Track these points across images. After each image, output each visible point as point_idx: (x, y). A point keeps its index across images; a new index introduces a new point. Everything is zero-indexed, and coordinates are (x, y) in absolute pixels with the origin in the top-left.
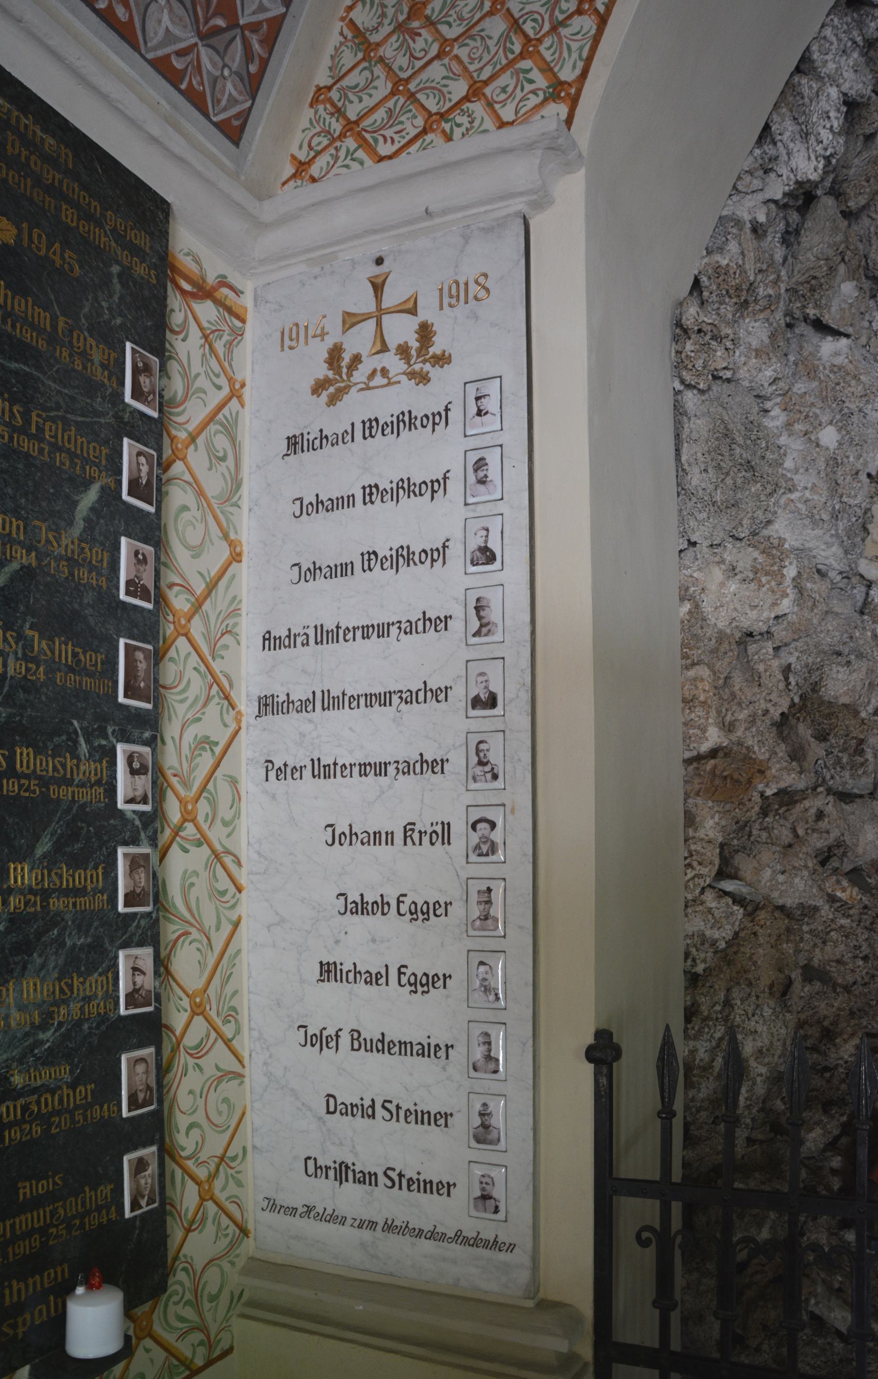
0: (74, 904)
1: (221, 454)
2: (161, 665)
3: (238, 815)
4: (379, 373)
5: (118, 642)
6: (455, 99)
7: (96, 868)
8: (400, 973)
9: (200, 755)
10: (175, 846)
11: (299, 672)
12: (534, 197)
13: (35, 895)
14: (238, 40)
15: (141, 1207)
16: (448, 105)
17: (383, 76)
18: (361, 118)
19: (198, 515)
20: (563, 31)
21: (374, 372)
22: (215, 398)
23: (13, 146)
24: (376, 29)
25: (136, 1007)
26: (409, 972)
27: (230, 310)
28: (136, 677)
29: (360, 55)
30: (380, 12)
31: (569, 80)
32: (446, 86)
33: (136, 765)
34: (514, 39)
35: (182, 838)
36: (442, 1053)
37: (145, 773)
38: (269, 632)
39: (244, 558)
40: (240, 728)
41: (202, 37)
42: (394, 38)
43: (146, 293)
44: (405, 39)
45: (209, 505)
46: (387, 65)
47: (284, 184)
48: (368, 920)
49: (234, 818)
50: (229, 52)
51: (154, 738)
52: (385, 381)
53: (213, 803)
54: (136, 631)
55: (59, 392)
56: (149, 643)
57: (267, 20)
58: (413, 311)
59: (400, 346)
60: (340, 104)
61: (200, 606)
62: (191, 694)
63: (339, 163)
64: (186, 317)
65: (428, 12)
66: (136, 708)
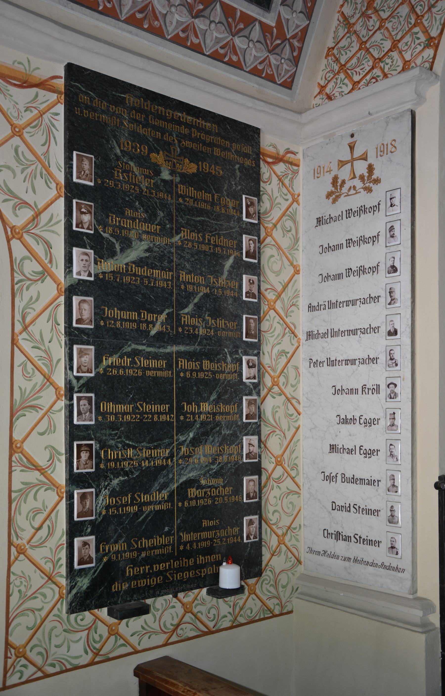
0: (225, 418)
1: (289, 229)
2: (262, 324)
3: (299, 382)
4: (352, 188)
6: (386, 50)
7: (234, 405)
8: (360, 449)
10: (269, 395)
11: (323, 321)
12: (415, 102)
14: (287, 46)
16: (383, 54)
17: (356, 41)
18: (347, 63)
19: (278, 258)
20: (434, 10)
21: (350, 188)
22: (285, 205)
23: (194, 134)
24: (353, 16)
25: (250, 459)
26: (363, 448)
27: (291, 163)
28: (250, 330)
29: (346, 30)
30: (354, 7)
31: (435, 36)
32: (382, 44)
33: (251, 364)
34: (412, 17)
35: (272, 392)
36: (376, 484)
37: (255, 367)
38: (310, 304)
39: (301, 272)
40: (299, 345)
41: (270, 51)
42: (361, 20)
43: (251, 172)
44: (365, 21)
45: (284, 253)
46: (357, 34)
47: (315, 97)
48: (348, 426)
49: (297, 384)
50: (283, 52)
51: (259, 353)
52: (355, 192)
53: (287, 378)
55: (216, 224)
56: (256, 315)
57: (300, 31)
58: (365, 159)
59: (360, 175)
60: (337, 56)
61: (280, 296)
62: (276, 333)
63: (338, 86)
64: (270, 174)
65: (375, 5)
66: (251, 342)
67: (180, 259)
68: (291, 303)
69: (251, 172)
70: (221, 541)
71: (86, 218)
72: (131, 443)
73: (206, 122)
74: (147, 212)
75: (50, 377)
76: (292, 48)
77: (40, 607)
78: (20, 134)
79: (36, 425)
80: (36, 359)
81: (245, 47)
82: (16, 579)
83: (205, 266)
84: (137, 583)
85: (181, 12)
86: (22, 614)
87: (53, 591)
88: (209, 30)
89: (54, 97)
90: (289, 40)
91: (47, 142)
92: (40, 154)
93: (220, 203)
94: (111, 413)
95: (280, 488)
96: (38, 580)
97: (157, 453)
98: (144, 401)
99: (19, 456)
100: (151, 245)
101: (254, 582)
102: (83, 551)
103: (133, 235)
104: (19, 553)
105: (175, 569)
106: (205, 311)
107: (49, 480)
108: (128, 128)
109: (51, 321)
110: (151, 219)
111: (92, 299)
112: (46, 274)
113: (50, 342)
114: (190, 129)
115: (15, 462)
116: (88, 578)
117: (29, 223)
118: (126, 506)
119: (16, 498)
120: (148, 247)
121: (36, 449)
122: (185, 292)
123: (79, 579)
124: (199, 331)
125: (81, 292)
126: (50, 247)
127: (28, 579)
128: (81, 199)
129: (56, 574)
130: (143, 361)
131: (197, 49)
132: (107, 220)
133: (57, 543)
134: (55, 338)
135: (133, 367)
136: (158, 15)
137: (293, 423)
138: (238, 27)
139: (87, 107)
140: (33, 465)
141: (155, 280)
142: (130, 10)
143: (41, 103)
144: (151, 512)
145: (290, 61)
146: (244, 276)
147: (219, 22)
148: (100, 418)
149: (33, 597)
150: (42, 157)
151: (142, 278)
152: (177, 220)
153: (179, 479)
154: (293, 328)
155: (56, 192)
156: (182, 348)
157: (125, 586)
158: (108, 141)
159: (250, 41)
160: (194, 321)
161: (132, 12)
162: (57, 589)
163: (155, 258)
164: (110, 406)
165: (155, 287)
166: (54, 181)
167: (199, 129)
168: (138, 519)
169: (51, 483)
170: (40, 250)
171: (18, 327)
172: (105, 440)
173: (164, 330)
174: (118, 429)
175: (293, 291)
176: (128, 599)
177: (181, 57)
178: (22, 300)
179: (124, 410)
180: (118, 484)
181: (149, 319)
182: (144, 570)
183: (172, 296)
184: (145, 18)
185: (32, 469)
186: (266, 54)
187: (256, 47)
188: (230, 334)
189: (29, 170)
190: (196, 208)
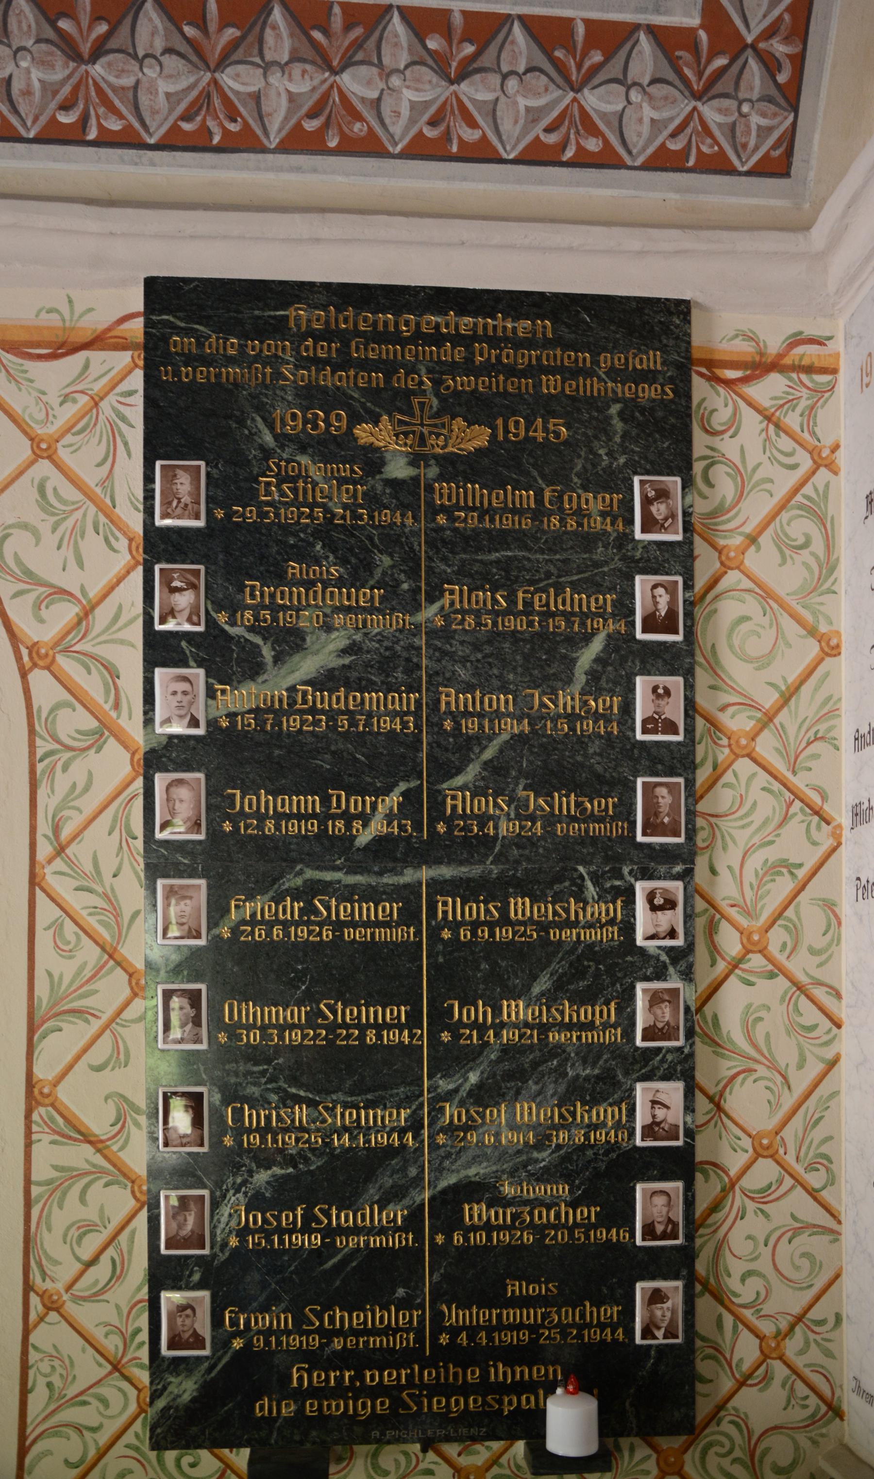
0: (579, 1038)
1: (801, 541)
5: (635, 782)
7: (607, 1003)
9: (773, 880)
10: (732, 979)
13: (532, 1029)
14: (753, 65)
15: (655, 1337)
22: (787, 481)
25: (656, 1139)
28: (656, 814)
33: (658, 901)
35: (744, 970)
40: (839, 844)
45: (782, 605)
49: (830, 945)
50: (743, 84)
53: (795, 932)
54: (660, 767)
57: (787, 10)
61: (771, 720)
62: (757, 818)
66: (661, 845)
67: (439, 661)
68: (811, 734)
69: (660, 414)
70: (564, 1334)
71: (184, 600)
72: (302, 1093)
73: (515, 319)
74: (343, 561)
75: (115, 949)
76: (771, 65)
77: (95, 1424)
78: (50, 452)
79: (85, 1050)
80: (84, 913)
81: (620, 107)
82: (42, 1360)
83: (515, 668)
84: (320, 1406)
85: (418, 80)
86: (55, 1431)
87: (125, 1394)
88: (503, 99)
89: (125, 358)
90: (753, 46)
91: (110, 456)
92: (93, 485)
93: (561, 509)
94: (249, 1027)
95: (766, 1216)
96: (89, 1369)
97: (375, 1117)
98: (339, 996)
99: (47, 1112)
100: (358, 637)
101: (676, 1446)
102: (179, 1321)
103: (307, 620)
104: (48, 1309)
105: (423, 1386)
106: (517, 778)
107: (114, 1166)
108: (295, 382)
109: (116, 833)
110: (356, 578)
111: (201, 776)
112: (107, 733)
113: (115, 876)
114: (469, 347)
115: (39, 1125)
116: (194, 1379)
117: (68, 633)
118: (291, 1232)
119: (40, 1196)
120: (348, 642)
121: (86, 1099)
122: (454, 736)
123: (172, 1379)
124: (496, 828)
125: (175, 763)
126: (115, 675)
127: (67, 1361)
128: (175, 562)
129: (131, 1360)
130: (337, 907)
131: (482, 154)
132: (239, 597)
133: (133, 1296)
134: (126, 867)
135: (308, 923)
136: (360, 107)
137: (818, 1051)
138: (587, 64)
139: (189, 359)
140: (79, 1132)
141: (370, 715)
142: (286, 119)
143: (96, 380)
144: (358, 1250)
145: (770, 100)
146: (639, 680)
147: (528, 70)
148: (222, 1037)
149: (79, 1400)
150: (98, 490)
151: (332, 715)
152: (430, 570)
153: (437, 1179)
154: (819, 801)
155: (129, 557)
156: (446, 872)
157: (288, 1409)
158: (242, 423)
159: (628, 88)
160: (480, 805)
161: (293, 122)
162: (132, 1393)
163: (368, 665)
164: (247, 1010)
165: (370, 733)
166: (125, 534)
167: (494, 341)
168: (321, 1264)
169: (119, 1170)
170: (92, 684)
171: (44, 849)
172: (236, 1084)
173: (396, 830)
174: (269, 1061)
175: (820, 697)
176: (297, 1438)
177: (441, 185)
178: (53, 791)
179: (285, 1018)
180: (268, 1183)
181: (352, 810)
182: (340, 1380)
183: (419, 749)
184: (327, 125)
185: (75, 1140)
186: (686, 106)
187: (651, 98)
188: (595, 828)
189: (69, 523)
190: (488, 532)
